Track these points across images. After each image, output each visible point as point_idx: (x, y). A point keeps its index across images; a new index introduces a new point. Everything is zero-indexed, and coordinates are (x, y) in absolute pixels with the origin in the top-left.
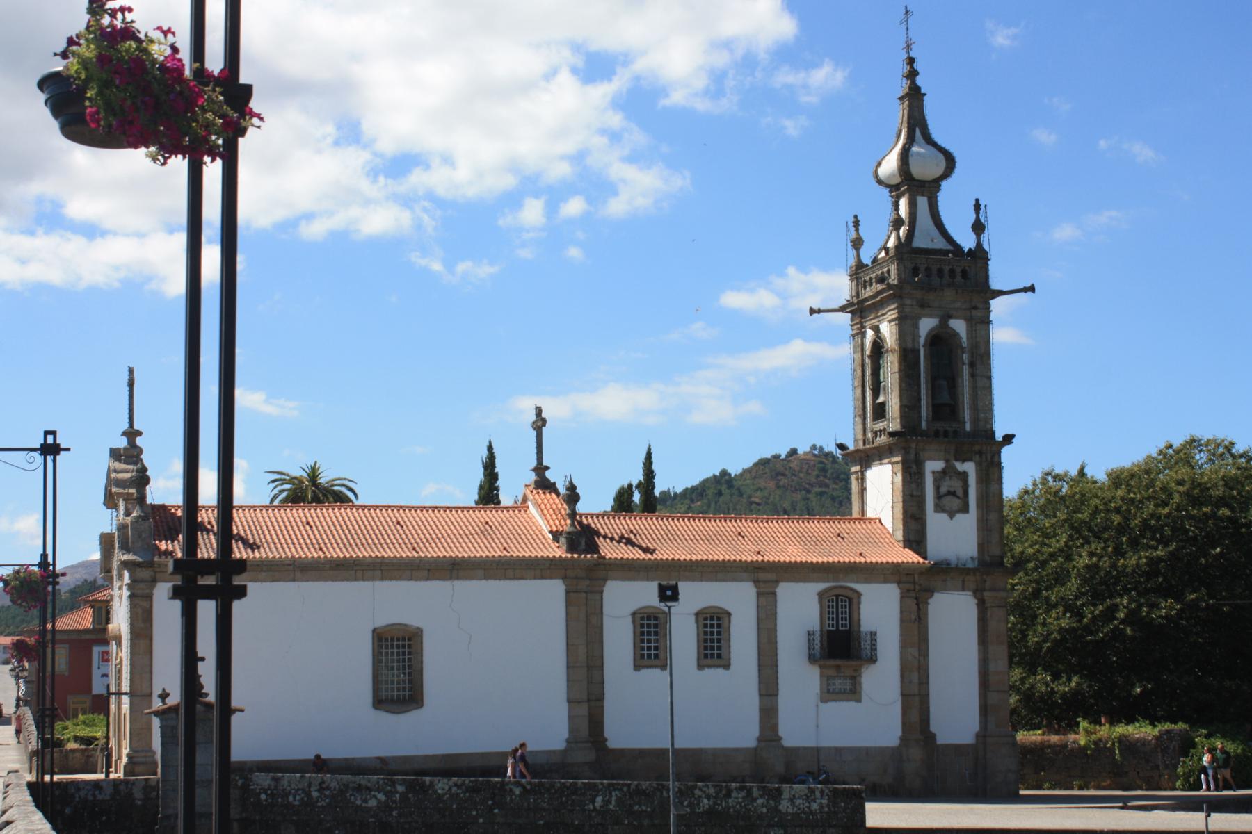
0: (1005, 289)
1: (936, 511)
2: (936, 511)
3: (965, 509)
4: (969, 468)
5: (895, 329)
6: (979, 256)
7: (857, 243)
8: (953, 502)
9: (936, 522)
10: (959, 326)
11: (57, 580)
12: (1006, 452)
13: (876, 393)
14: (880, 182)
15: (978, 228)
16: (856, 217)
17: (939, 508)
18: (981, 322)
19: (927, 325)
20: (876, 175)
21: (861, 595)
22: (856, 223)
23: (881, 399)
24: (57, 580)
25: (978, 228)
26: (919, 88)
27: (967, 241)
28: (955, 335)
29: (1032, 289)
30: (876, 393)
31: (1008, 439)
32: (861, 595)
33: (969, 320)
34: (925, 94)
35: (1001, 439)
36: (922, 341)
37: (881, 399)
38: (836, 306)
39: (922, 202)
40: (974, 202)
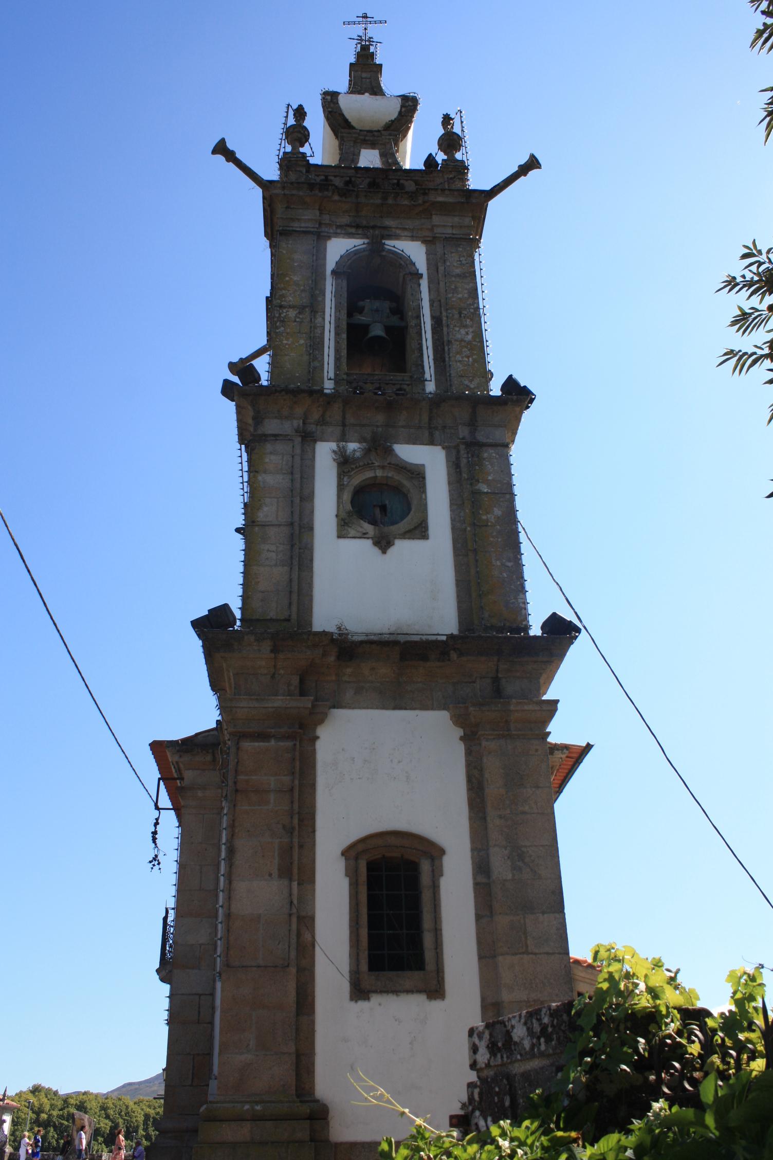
3: (420, 531)
15: (436, 154)
28: (403, 264)
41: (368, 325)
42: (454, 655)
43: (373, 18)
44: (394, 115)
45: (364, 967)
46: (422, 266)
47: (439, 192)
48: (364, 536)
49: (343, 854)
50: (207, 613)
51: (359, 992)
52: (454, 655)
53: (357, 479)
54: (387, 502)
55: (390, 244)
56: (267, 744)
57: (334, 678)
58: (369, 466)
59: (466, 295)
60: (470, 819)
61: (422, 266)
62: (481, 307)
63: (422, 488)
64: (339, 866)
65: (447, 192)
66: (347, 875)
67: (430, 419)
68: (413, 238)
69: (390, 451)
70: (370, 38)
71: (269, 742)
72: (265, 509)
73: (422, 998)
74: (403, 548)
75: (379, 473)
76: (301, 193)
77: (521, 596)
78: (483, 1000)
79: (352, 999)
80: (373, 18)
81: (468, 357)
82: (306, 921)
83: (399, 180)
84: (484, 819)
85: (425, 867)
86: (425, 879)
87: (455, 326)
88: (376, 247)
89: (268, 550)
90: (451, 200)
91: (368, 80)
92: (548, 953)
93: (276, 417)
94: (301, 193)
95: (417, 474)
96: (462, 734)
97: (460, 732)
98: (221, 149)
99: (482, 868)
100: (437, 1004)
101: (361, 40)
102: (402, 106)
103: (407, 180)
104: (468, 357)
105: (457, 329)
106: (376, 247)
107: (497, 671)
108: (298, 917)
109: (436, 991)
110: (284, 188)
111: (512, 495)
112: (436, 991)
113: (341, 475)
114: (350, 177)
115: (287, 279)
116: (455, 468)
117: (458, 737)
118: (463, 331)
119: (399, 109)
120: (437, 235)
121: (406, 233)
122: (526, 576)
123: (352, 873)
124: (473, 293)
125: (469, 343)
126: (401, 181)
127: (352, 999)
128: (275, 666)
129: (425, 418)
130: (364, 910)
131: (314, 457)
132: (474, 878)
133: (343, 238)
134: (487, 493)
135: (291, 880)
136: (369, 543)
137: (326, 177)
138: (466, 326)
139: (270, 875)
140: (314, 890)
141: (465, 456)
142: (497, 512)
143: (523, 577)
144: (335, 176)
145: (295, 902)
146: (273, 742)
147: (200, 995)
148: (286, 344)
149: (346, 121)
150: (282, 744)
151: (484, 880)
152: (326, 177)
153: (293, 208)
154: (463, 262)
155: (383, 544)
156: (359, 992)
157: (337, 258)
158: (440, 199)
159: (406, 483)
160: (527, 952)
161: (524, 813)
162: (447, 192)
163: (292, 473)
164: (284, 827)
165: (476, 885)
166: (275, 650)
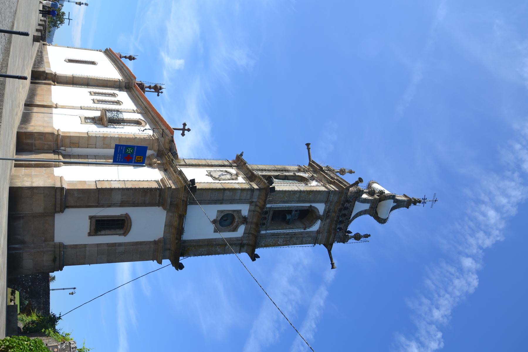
0: (332, 252)
4: (242, 229)
10: (316, 227)
12: (244, 256)
13: (277, 177)
15: (357, 237)
18: (314, 240)
19: (321, 208)
25: (357, 237)
30: (277, 177)
31: (254, 257)
33: (318, 232)
34: (214, 222)
35: (255, 253)
38: (312, 159)
40: (368, 234)
41: (291, 214)
42: (177, 241)
43: (435, 203)
44: (379, 216)
45: (97, 219)
46: (311, 229)
47: (334, 237)
48: (217, 217)
49: (127, 214)
50: (163, 260)
51: (91, 218)
52: (177, 241)
53: (235, 214)
54: (228, 221)
55: (319, 222)
56: (158, 196)
57: (175, 211)
58: (239, 218)
59: (294, 242)
60: (133, 242)
61: (311, 229)
62: (289, 246)
63: (230, 231)
64: (124, 213)
65: (333, 239)
66: (121, 214)
67: (252, 234)
68: (320, 228)
69: (243, 223)
70: (426, 203)
71: (159, 197)
72: (229, 193)
73: (89, 231)
74: (212, 227)
75: (236, 220)
76: (343, 198)
77: (193, 255)
78: (87, 244)
79: (89, 216)
80: (435, 203)
81: (272, 242)
82: (110, 206)
83: (345, 223)
84: (133, 245)
85: (122, 232)
86: (118, 231)
87: (284, 239)
88: (318, 217)
89: (215, 194)
90: (330, 240)
91: (403, 204)
92: (97, 260)
93: (259, 194)
94: (343, 198)
95: (235, 230)
96: (156, 240)
97: (157, 240)
98: (308, 145)
99: (120, 244)
100: (87, 234)
101: (424, 199)
102: (382, 219)
103: (344, 225)
104: (272, 242)
105: (283, 240)
106: (318, 217)
107: (172, 250)
108: (111, 205)
109: (90, 234)
110: (346, 193)
111: (223, 254)
112: (90, 234)
114: (349, 209)
115: (311, 193)
116: (237, 239)
117: (155, 239)
118: (282, 241)
119: (381, 218)
120: (319, 234)
121: (322, 226)
122: (199, 257)
123: (121, 216)
124: (295, 244)
125: (277, 243)
126: (344, 223)
127: (89, 216)
128: (179, 199)
129: (253, 232)
130: (111, 219)
131: (245, 204)
132: (117, 243)
133: (325, 208)
134: (225, 248)
135: (121, 204)
136: (215, 218)
137: (351, 202)
138: (283, 242)
139: (122, 199)
140: (118, 207)
141: (238, 243)
142: (219, 250)
143: (198, 256)
144: (351, 205)
145: (115, 205)
146: (158, 198)
147: (96, 145)
148: (286, 194)
149: (381, 201)
150: (158, 200)
151: (117, 245)
152: (351, 202)
153: (339, 194)
154: (307, 242)
155: (214, 222)
156: (91, 218)
157: (315, 206)
158: (331, 237)
159: (232, 227)
160: (98, 255)
161: (133, 255)
162: (333, 239)
163: (239, 200)
164: (134, 201)
165: (116, 243)
166: (183, 200)
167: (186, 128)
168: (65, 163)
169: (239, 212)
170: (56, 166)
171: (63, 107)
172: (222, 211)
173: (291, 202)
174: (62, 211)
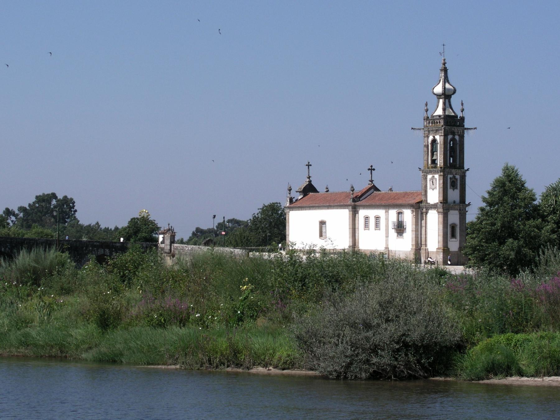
1: (450, 189)
2: (450, 189)
3: (457, 188)
5: (442, 138)
6: (463, 119)
7: (427, 111)
8: (454, 185)
9: (450, 191)
11: (109, 229)
13: (433, 155)
14: (434, 94)
15: (462, 110)
16: (427, 102)
17: (431, 188)
18: (462, 137)
20: (433, 92)
21: (198, 230)
22: (462, 104)
23: (434, 158)
24: (109, 229)
25: (462, 110)
26: (446, 68)
27: (460, 114)
29: (412, 129)
31: (468, 170)
32: (198, 230)
36: (430, 143)
37: (434, 158)
39: (447, 100)
74: (455, 190)
95: (457, 180)
113: (450, 180)
116: (460, 178)
167: (371, 168)
168: (426, 245)
169: (450, 178)
170: (428, 250)
171: (387, 244)
172: (450, 187)
173: (447, 148)
174: (449, 249)
